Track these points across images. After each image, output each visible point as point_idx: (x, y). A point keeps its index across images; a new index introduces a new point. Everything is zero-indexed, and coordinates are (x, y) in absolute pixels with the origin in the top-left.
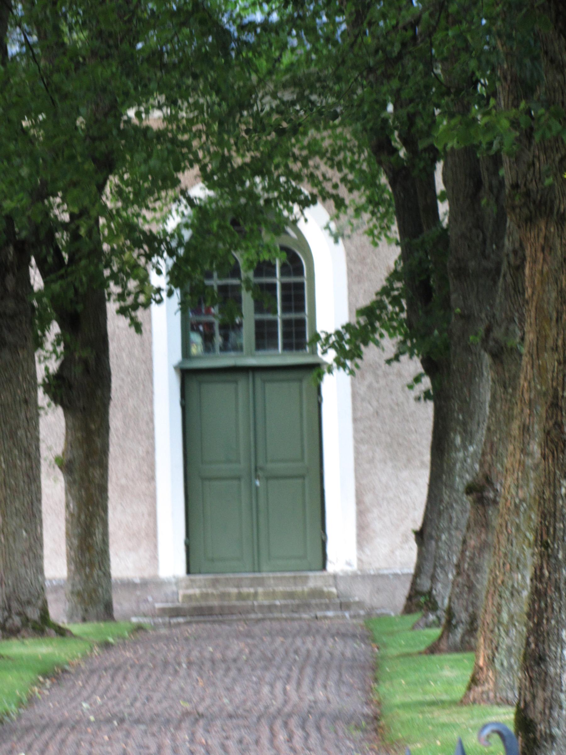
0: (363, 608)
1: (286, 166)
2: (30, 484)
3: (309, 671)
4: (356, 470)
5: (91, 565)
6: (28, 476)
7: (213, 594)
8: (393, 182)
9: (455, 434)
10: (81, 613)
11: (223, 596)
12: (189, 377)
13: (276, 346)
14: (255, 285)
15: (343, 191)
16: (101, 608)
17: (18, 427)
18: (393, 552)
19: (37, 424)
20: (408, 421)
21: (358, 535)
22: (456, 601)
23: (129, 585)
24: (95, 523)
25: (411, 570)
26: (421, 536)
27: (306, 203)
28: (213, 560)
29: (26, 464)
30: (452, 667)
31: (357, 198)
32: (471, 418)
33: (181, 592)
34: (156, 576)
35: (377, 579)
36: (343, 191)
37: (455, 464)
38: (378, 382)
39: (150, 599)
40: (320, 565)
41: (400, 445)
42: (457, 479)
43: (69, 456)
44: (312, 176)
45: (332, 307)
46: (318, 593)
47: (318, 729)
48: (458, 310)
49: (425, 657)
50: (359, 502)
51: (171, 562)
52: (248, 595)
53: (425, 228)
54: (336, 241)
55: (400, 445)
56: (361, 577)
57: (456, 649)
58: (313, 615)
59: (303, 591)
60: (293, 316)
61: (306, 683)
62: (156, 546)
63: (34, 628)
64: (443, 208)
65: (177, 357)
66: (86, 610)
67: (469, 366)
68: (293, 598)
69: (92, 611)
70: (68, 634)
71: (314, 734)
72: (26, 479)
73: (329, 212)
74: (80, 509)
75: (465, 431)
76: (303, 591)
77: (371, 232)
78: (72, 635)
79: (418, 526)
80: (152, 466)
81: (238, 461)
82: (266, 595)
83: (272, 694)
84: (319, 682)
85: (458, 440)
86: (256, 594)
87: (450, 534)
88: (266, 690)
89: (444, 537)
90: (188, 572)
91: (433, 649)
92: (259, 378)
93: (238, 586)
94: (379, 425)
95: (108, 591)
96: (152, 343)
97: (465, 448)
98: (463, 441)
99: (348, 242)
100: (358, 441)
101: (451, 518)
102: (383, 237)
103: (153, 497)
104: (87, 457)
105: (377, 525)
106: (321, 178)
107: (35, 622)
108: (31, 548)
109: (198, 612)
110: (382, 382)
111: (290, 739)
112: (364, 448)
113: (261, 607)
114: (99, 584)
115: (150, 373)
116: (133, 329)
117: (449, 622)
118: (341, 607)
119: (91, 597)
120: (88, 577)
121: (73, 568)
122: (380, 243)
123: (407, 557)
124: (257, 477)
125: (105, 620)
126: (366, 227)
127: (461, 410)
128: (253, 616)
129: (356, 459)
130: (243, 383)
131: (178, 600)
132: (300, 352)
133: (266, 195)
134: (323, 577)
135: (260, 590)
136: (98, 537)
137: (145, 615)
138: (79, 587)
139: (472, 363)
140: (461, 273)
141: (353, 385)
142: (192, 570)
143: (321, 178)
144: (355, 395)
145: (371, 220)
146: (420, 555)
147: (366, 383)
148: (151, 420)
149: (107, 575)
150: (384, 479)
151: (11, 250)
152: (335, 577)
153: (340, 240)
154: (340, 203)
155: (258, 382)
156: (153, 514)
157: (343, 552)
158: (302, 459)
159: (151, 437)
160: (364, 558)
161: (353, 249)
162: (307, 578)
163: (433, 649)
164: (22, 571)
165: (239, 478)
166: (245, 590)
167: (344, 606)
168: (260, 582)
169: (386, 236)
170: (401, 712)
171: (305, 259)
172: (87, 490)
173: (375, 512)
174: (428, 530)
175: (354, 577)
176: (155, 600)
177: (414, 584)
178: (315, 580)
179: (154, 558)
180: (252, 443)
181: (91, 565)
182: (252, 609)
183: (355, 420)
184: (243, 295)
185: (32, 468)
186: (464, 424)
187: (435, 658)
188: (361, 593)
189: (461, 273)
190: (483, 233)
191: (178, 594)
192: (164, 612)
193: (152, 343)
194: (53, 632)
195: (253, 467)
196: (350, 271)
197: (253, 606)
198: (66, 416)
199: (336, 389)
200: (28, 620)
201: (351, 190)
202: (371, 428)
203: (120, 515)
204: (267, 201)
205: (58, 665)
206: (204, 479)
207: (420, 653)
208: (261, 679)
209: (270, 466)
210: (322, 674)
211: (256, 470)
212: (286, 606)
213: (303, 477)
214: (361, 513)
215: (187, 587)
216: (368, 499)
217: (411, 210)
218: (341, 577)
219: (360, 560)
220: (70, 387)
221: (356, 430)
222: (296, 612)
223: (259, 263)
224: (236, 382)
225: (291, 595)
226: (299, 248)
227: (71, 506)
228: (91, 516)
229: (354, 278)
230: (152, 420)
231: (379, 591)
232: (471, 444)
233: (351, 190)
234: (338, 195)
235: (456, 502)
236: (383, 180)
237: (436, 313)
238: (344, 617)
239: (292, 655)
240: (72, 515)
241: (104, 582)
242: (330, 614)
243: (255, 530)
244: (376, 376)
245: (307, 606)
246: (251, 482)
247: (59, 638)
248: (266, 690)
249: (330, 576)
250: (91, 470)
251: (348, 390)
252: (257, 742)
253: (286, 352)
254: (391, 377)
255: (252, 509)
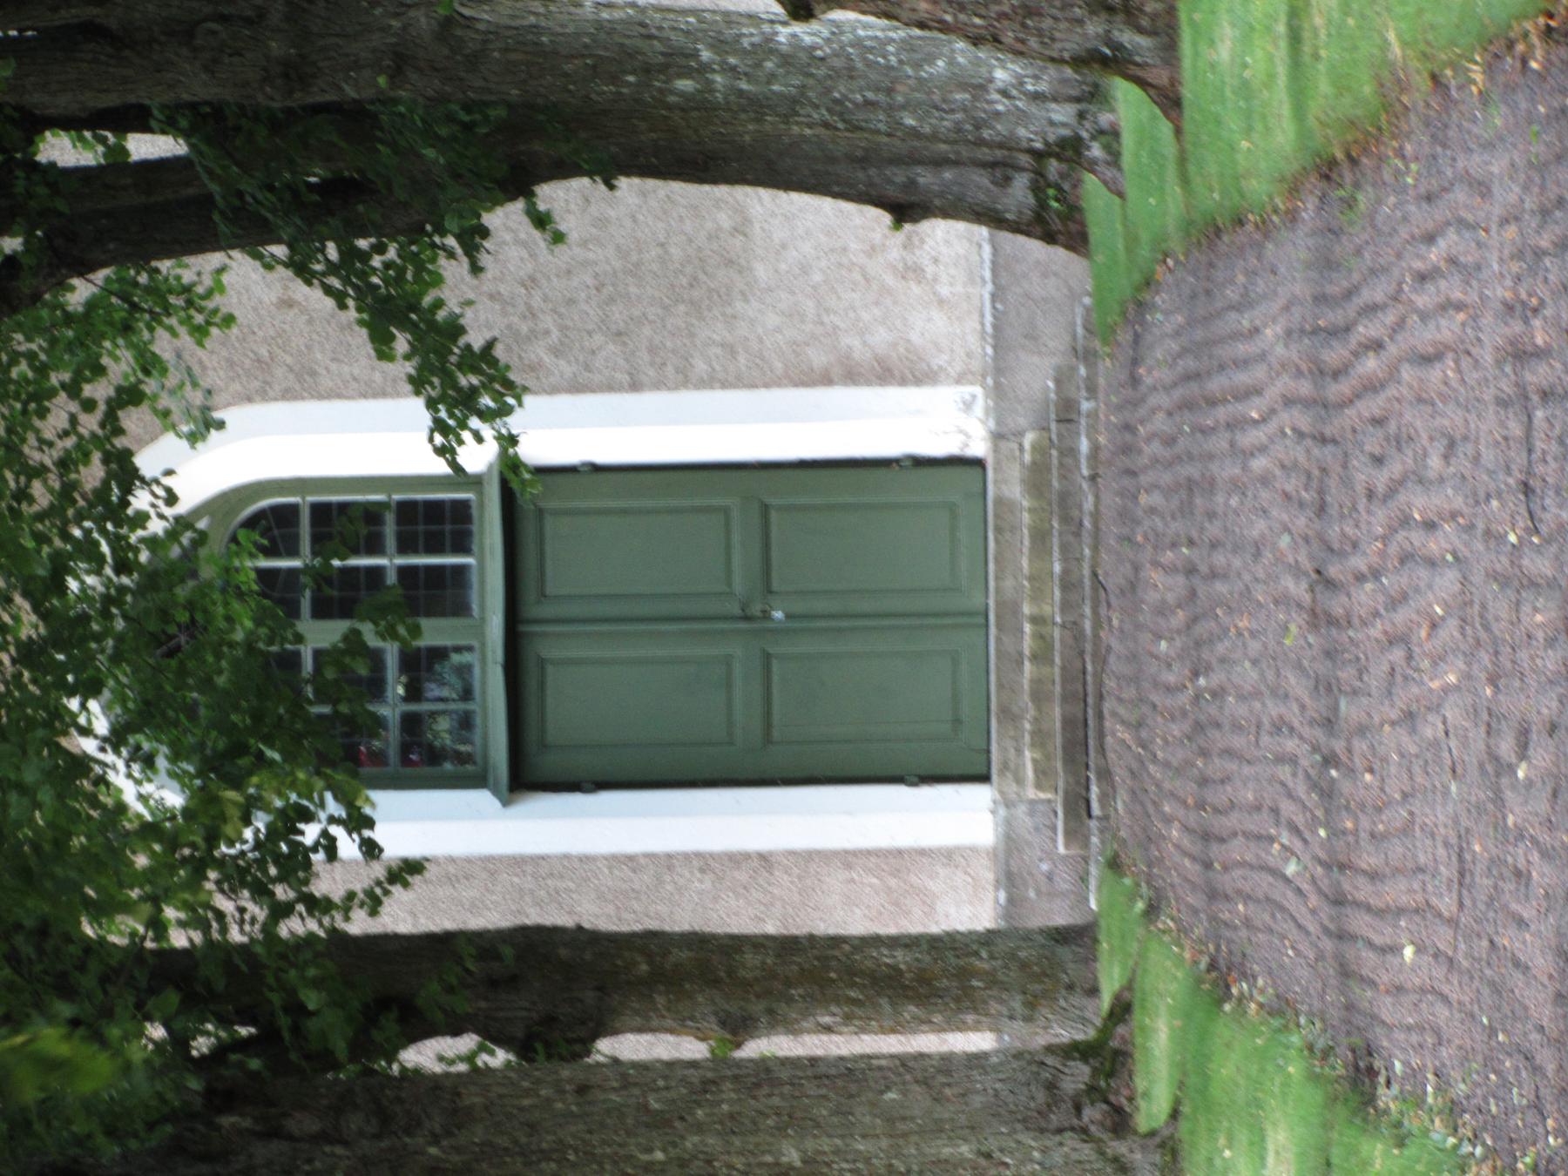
0: (1073, 369)
1: (40, 517)
2: (775, 1082)
3: (1215, 385)
4: (753, 386)
5: (964, 974)
6: (758, 1085)
7: (1036, 720)
8: (84, 268)
9: (672, 92)
10: (1077, 999)
11: (1039, 695)
12: (527, 775)
13: (460, 571)
14: (315, 554)
15: (100, 391)
16: (1064, 953)
17: (645, 1108)
18: (941, 302)
19: (635, 1065)
20: (637, 265)
21: (903, 382)
22: (1058, 45)
23: (1014, 902)
24: (869, 963)
25: (983, 231)
26: (905, 211)
27: (125, 474)
28: (957, 721)
29: (728, 1091)
30: (1212, 43)
31: (120, 365)
32: (632, 54)
33: (1031, 793)
34: (993, 853)
35: (1004, 339)
36: (100, 391)
37: (741, 93)
38: (547, 332)
39: (1045, 867)
40: (974, 472)
41: (694, 282)
42: (775, 88)
43: (712, 1025)
44: (64, 464)
45: (374, 439)
46: (1037, 477)
47: (1349, 294)
48: (382, 81)
49: (1188, 112)
50: (826, 380)
51: (960, 817)
52: (1039, 637)
53: (191, 191)
54: (220, 425)
55: (694, 282)
56: (999, 378)
57: (1170, 47)
58: (1085, 486)
59: (1030, 510)
60: (390, 529)
61: (1242, 378)
62: (922, 852)
63: (1110, 1075)
64: (145, 147)
65: (482, 799)
66: (1070, 987)
67: (513, 56)
68: (1049, 532)
69: (1073, 971)
70: (1126, 994)
71: (1368, 295)
72: (766, 1090)
73: (154, 438)
74: (837, 1000)
75: (664, 68)
76: (1030, 510)
77: (200, 332)
78: (1129, 986)
79: (886, 218)
80: (736, 859)
81: (728, 661)
82: (1037, 596)
83: (1270, 439)
84: (1242, 349)
85: (685, 85)
86: (1036, 620)
87: (903, 107)
88: (1259, 464)
89: (910, 121)
90: (984, 778)
91: (1170, 101)
92: (531, 735)
93: (1018, 667)
94: (647, 331)
95: (1027, 937)
96: (451, 849)
97: (704, 68)
98: (687, 73)
99: (217, 399)
100: (685, 379)
101: (868, 103)
102: (210, 305)
103: (809, 858)
104: (715, 982)
105: (880, 338)
106: (70, 442)
107: (1095, 1072)
108: (925, 1083)
109: (1078, 749)
110: (548, 321)
111: (1377, 346)
112: (700, 366)
113: (1066, 606)
114: (1012, 956)
115: (518, 862)
116: (415, 880)
117: (1105, 62)
118: (1069, 421)
119: (1038, 978)
120: (992, 981)
121: (970, 1018)
122: (224, 310)
123: (950, 243)
124: (766, 616)
125: (1096, 941)
126: (186, 340)
127: (614, 79)
128: (1088, 626)
129: (725, 385)
130: (547, 647)
131: (1049, 801)
132: (475, 512)
133: (108, 571)
134: (998, 463)
135: (1027, 609)
136: (901, 957)
137: (1084, 879)
138: (1017, 1004)
139: (506, 50)
140: (294, 73)
141: (554, 390)
142: (982, 770)
143: (70, 442)
144: (577, 387)
145: (171, 329)
146: (947, 213)
147: (547, 359)
148: (629, 861)
149: (988, 938)
150: (772, 320)
151: (227, 1121)
152: (997, 437)
153: (217, 415)
154: (130, 396)
155: (547, 610)
156: (848, 858)
157: (937, 420)
158: (726, 511)
159: (668, 862)
160: (958, 367)
161: (236, 386)
162: (999, 501)
163: (1170, 101)
164: (977, 1101)
165: (767, 658)
166: (1027, 645)
167: (1066, 413)
168: (1009, 610)
169: (209, 294)
170: (1314, 108)
171: (254, 502)
172: (788, 983)
173: (851, 341)
174: (892, 192)
175: (1000, 394)
176: (1050, 855)
177: (1016, 228)
178: (1007, 485)
179: (948, 855)
180: (684, 626)
181: (964, 974)
182: (1073, 628)
183: (635, 386)
184: (341, 640)
185: (736, 1078)
186: (647, 70)
187: (1187, 93)
188: (1037, 376)
189: (294, 73)
190: (205, 20)
191: (1032, 802)
192: (1075, 833)
193: (451, 849)
194: (1121, 1030)
195: (742, 625)
196: (288, 395)
197: (1063, 626)
198: (615, 1032)
199: (558, 430)
200: (1092, 1089)
201: (100, 371)
202: (652, 350)
203: (848, 914)
204: (122, 567)
205: (1199, 981)
206: (768, 739)
207: (1178, 131)
208: (1236, 486)
209: (738, 586)
210: (1225, 352)
211: (747, 618)
212: (1064, 548)
213: (765, 509)
214: (851, 374)
215: (1019, 781)
216: (818, 358)
217: (147, 221)
218: (999, 422)
219: (959, 380)
220: (550, 1020)
221: (659, 385)
222: (1081, 524)
223: (264, 595)
224: (542, 663)
225: (1040, 537)
226: (234, 511)
227: (827, 1020)
228: (851, 973)
229: (304, 383)
230: (630, 860)
231: (1032, 336)
232: (695, 55)
233: (100, 371)
234: (109, 402)
235: (829, 90)
236: (80, 292)
237: (391, 168)
238: (1093, 415)
239: (1182, 443)
240: (848, 1019)
241: (1002, 946)
242: (1084, 446)
243: (886, 622)
244: (533, 335)
245: (1066, 503)
246: (779, 626)
247: (1137, 1014)
248: (1259, 464)
249: (996, 450)
250: (742, 973)
251: (564, 401)
252: (1378, 422)
253: (475, 548)
254: (537, 301)
255: (840, 630)
